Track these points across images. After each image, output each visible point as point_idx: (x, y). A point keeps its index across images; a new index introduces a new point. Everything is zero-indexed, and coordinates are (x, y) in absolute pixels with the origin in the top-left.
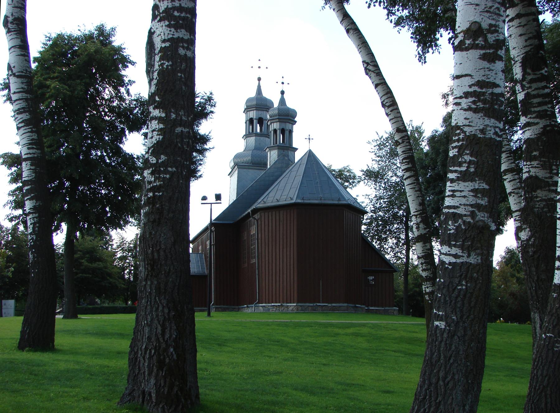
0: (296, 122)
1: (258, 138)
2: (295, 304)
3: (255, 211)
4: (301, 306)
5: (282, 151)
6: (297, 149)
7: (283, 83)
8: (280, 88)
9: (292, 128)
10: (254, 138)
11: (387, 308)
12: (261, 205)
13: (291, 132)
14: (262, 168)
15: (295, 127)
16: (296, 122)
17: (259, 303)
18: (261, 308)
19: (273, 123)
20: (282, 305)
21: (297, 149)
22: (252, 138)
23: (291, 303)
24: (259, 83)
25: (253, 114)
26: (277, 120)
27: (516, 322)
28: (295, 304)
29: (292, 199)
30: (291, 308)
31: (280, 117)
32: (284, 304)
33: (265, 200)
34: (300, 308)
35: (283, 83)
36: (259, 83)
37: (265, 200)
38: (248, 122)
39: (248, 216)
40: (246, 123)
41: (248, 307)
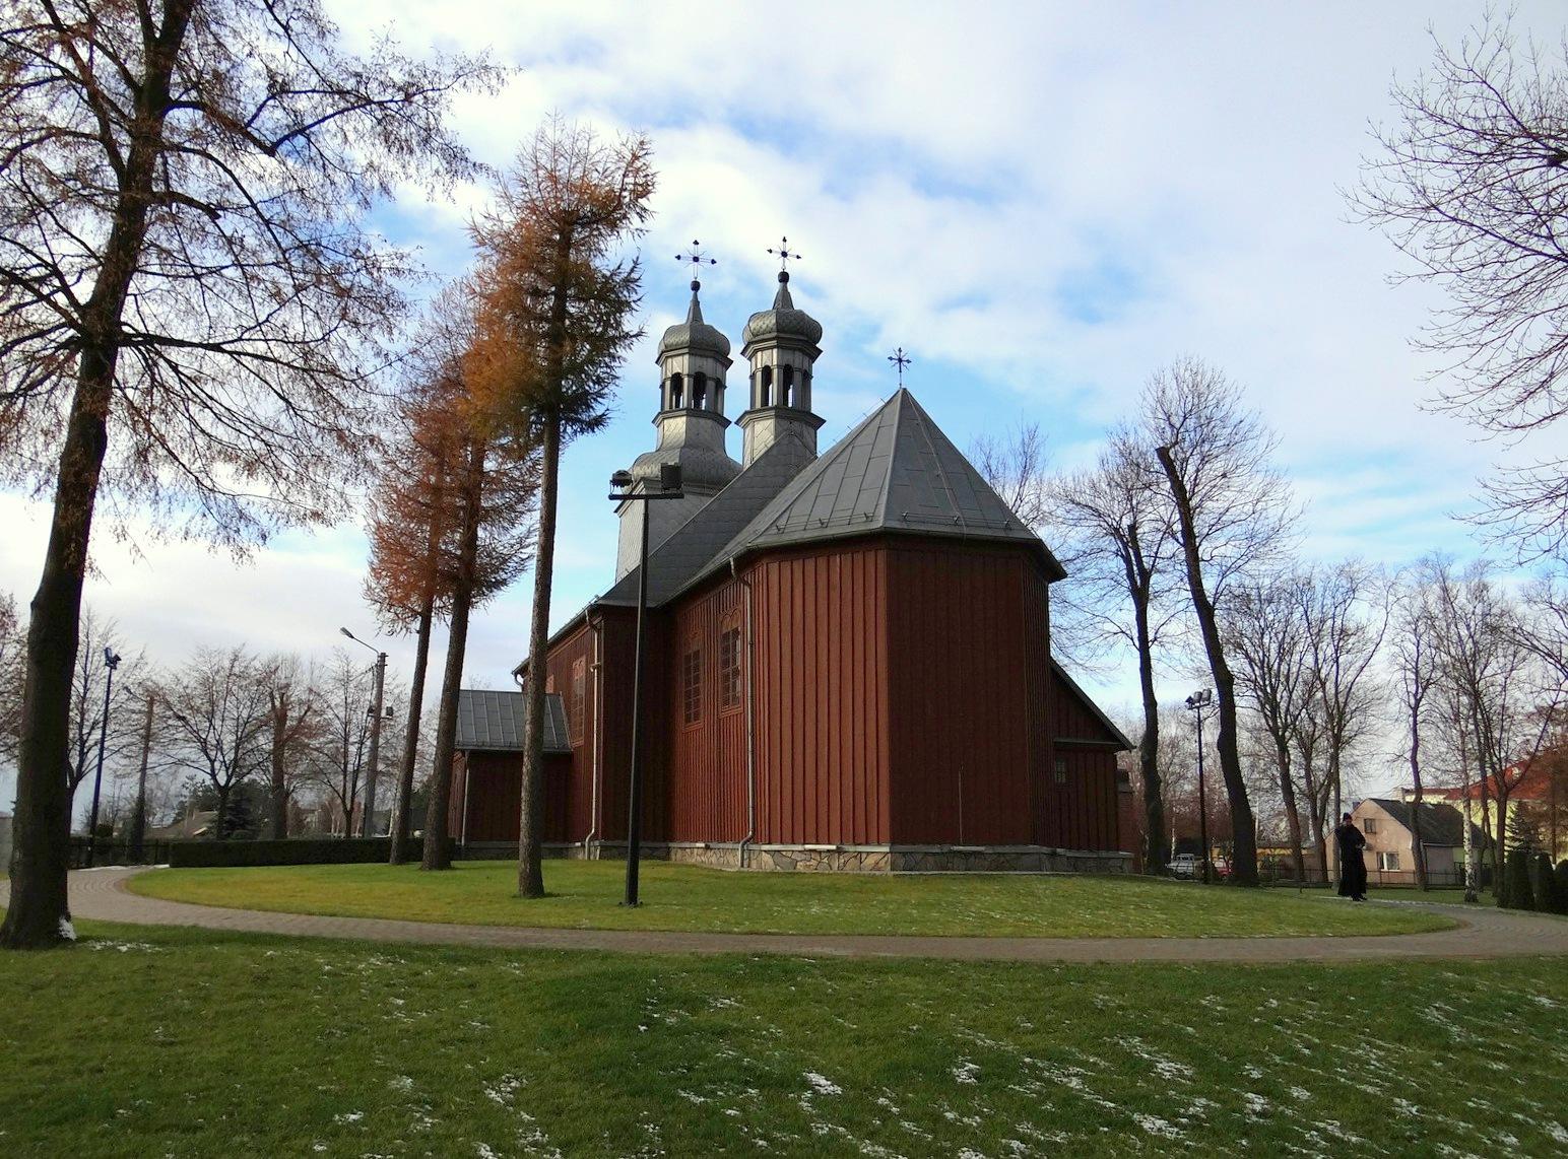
0: (820, 352)
1: (694, 420)
2: (886, 849)
3: (751, 558)
4: (904, 854)
5: (785, 424)
6: (824, 421)
7: (784, 254)
8: (776, 265)
9: (810, 366)
10: (684, 418)
11: (1104, 854)
12: (772, 539)
13: (807, 376)
14: (706, 491)
15: (818, 367)
16: (820, 352)
17: (755, 839)
18: (766, 857)
19: (762, 350)
20: (839, 851)
21: (824, 421)
22: (678, 419)
23: (867, 843)
24: (695, 296)
25: (681, 364)
26: (774, 342)
27: (68, 756)
28: (886, 849)
29: (869, 518)
30: (870, 861)
31: (782, 335)
32: (846, 848)
33: (782, 523)
34: (901, 861)
35: (784, 254)
36: (695, 296)
37: (782, 523)
38: (668, 383)
39: (722, 575)
40: (663, 386)
41: (707, 848)
